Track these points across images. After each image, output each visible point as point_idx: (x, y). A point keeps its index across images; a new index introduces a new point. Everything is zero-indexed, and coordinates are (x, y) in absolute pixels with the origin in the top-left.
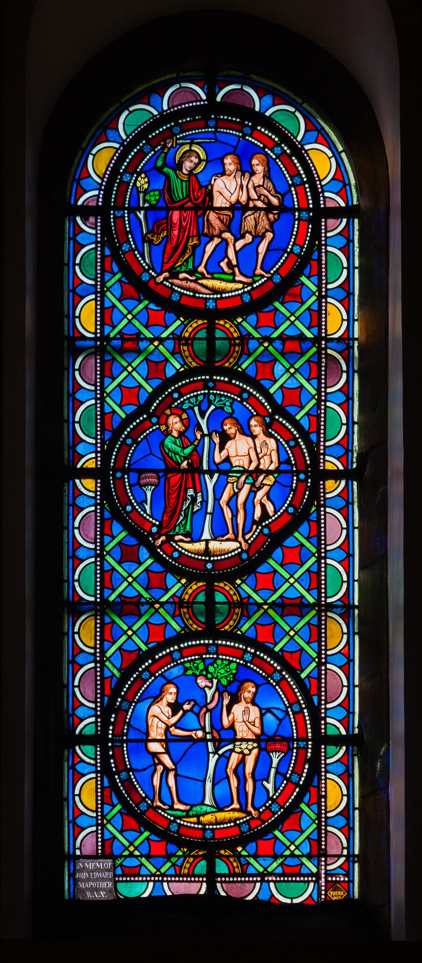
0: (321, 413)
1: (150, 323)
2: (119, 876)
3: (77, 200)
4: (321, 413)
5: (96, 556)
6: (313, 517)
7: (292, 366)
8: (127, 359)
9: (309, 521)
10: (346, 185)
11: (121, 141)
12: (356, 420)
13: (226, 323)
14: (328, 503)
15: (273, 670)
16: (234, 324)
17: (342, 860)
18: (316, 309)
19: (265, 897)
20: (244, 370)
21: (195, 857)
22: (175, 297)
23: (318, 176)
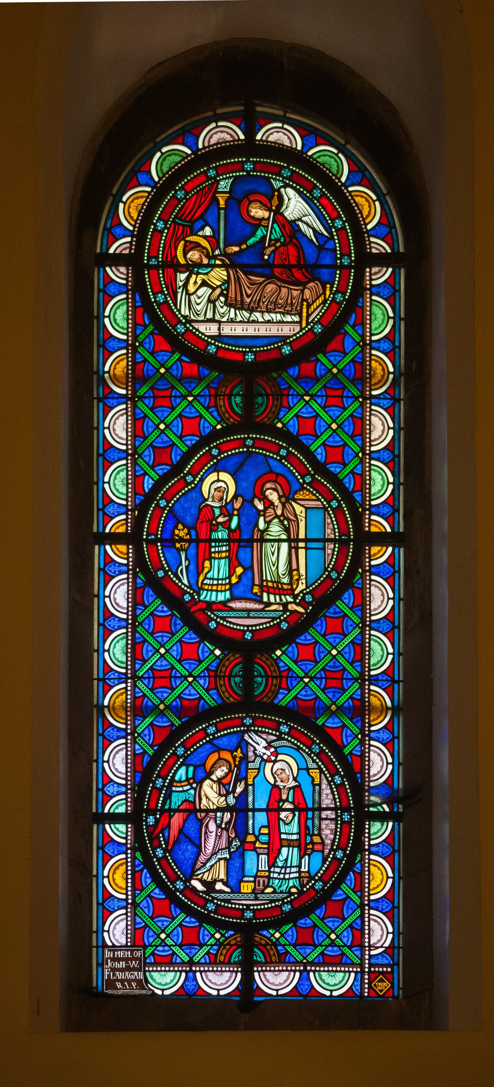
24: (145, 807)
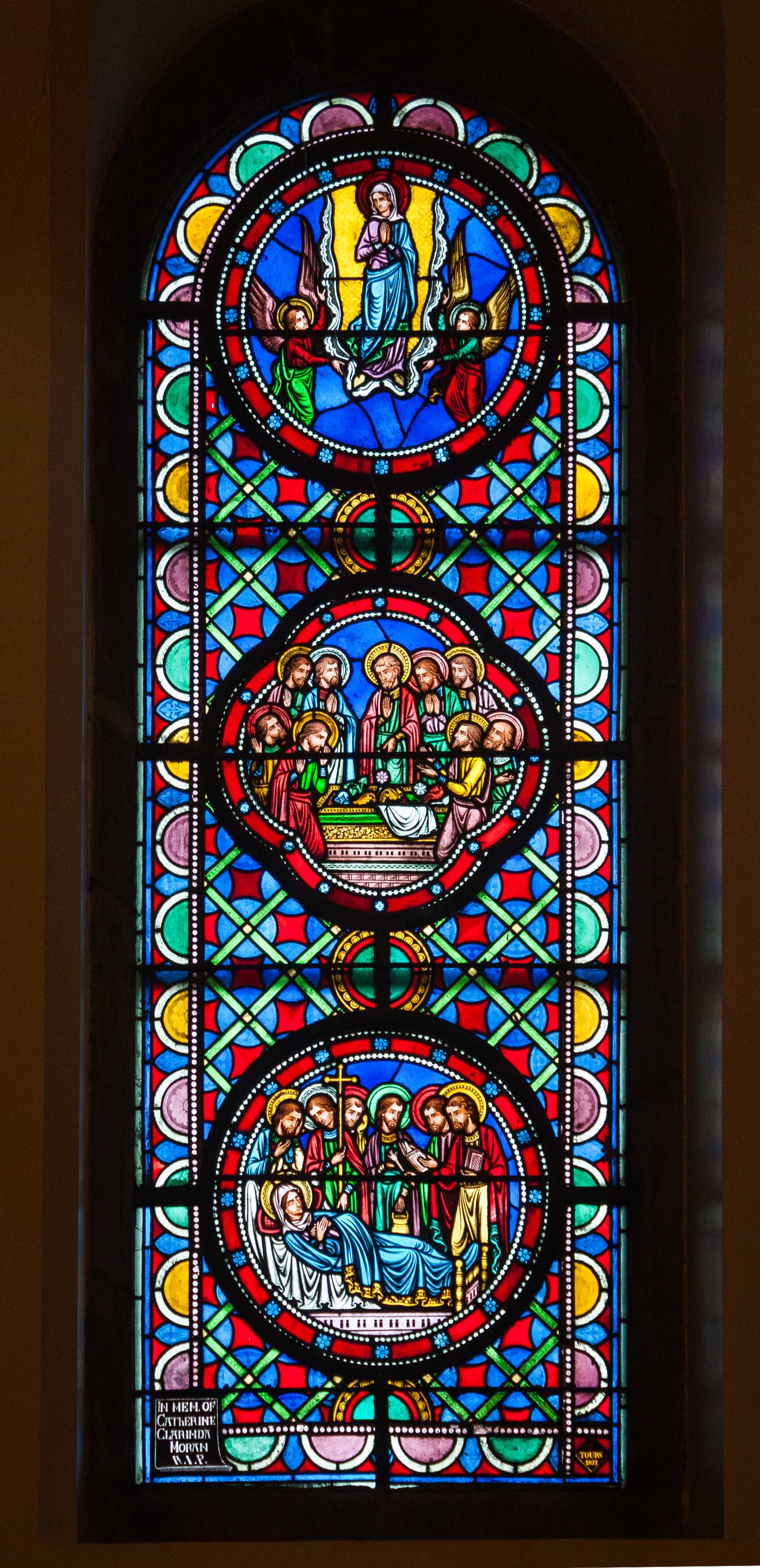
0: (565, 1130)
2: (228, 1427)
3: (158, 293)
5: (190, 889)
8: (244, 559)
9: (546, 828)
14: (577, 1151)
16: (423, 502)
17: (600, 1397)
18: (556, 1000)
20: (439, 580)
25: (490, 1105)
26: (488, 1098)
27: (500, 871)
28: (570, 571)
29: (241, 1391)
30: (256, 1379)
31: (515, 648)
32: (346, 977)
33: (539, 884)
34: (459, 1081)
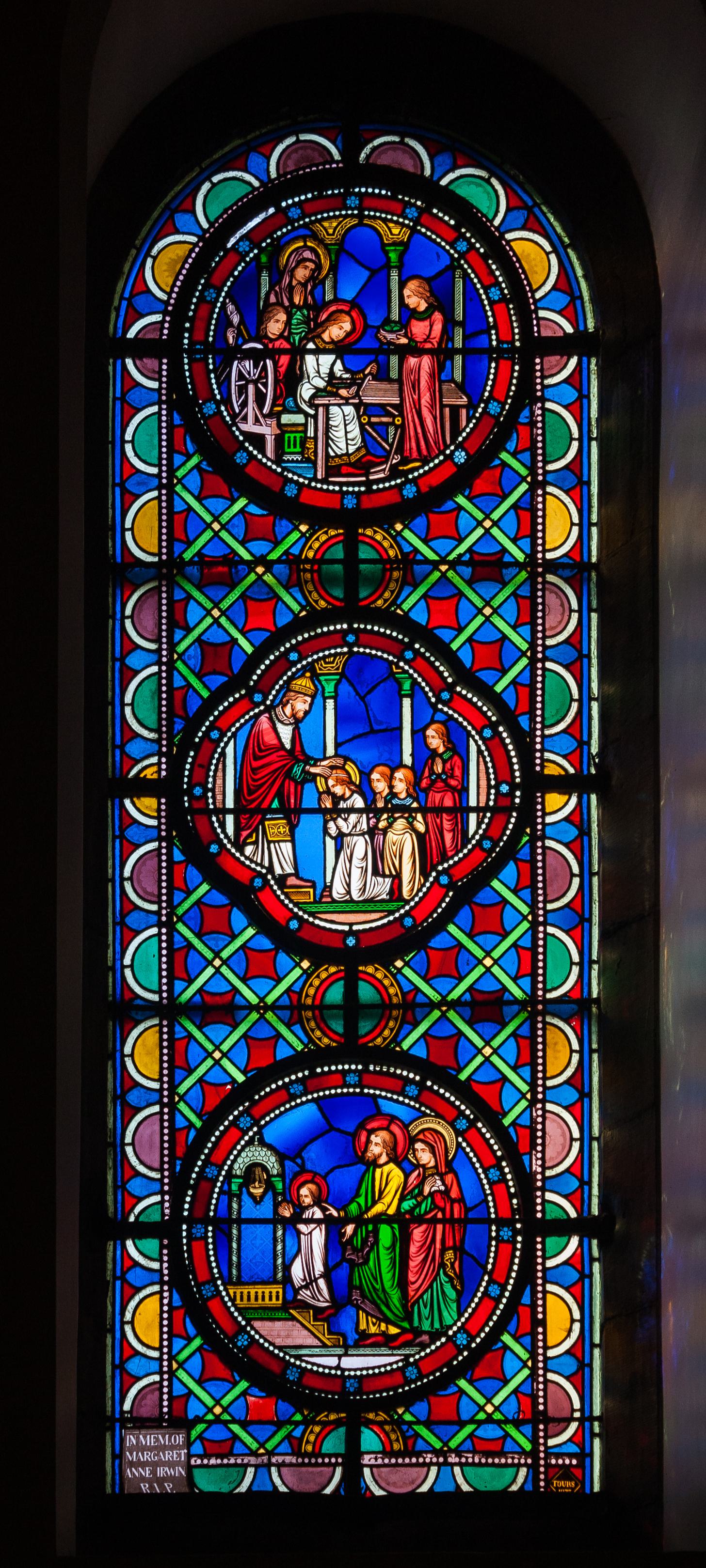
0: (538, 1390)
1: (249, 602)
4: (538, 1390)
6: (524, 853)
7: (487, 517)
10: (575, 297)
11: (200, 233)
12: (595, 957)
13: (375, 532)
15: (455, 1113)
17: (574, 1426)
19: (446, 1487)
20: (406, 614)
21: (324, 1424)
22: (291, 491)
23: (529, 284)
24: (186, 1213)
25: (460, 1139)
26: (458, 1133)
27: (470, 903)
28: (540, 864)
29: (210, 1423)
30: (225, 1410)
31: (484, 679)
32: (315, 575)
33: (509, 917)
34: (429, 1115)
